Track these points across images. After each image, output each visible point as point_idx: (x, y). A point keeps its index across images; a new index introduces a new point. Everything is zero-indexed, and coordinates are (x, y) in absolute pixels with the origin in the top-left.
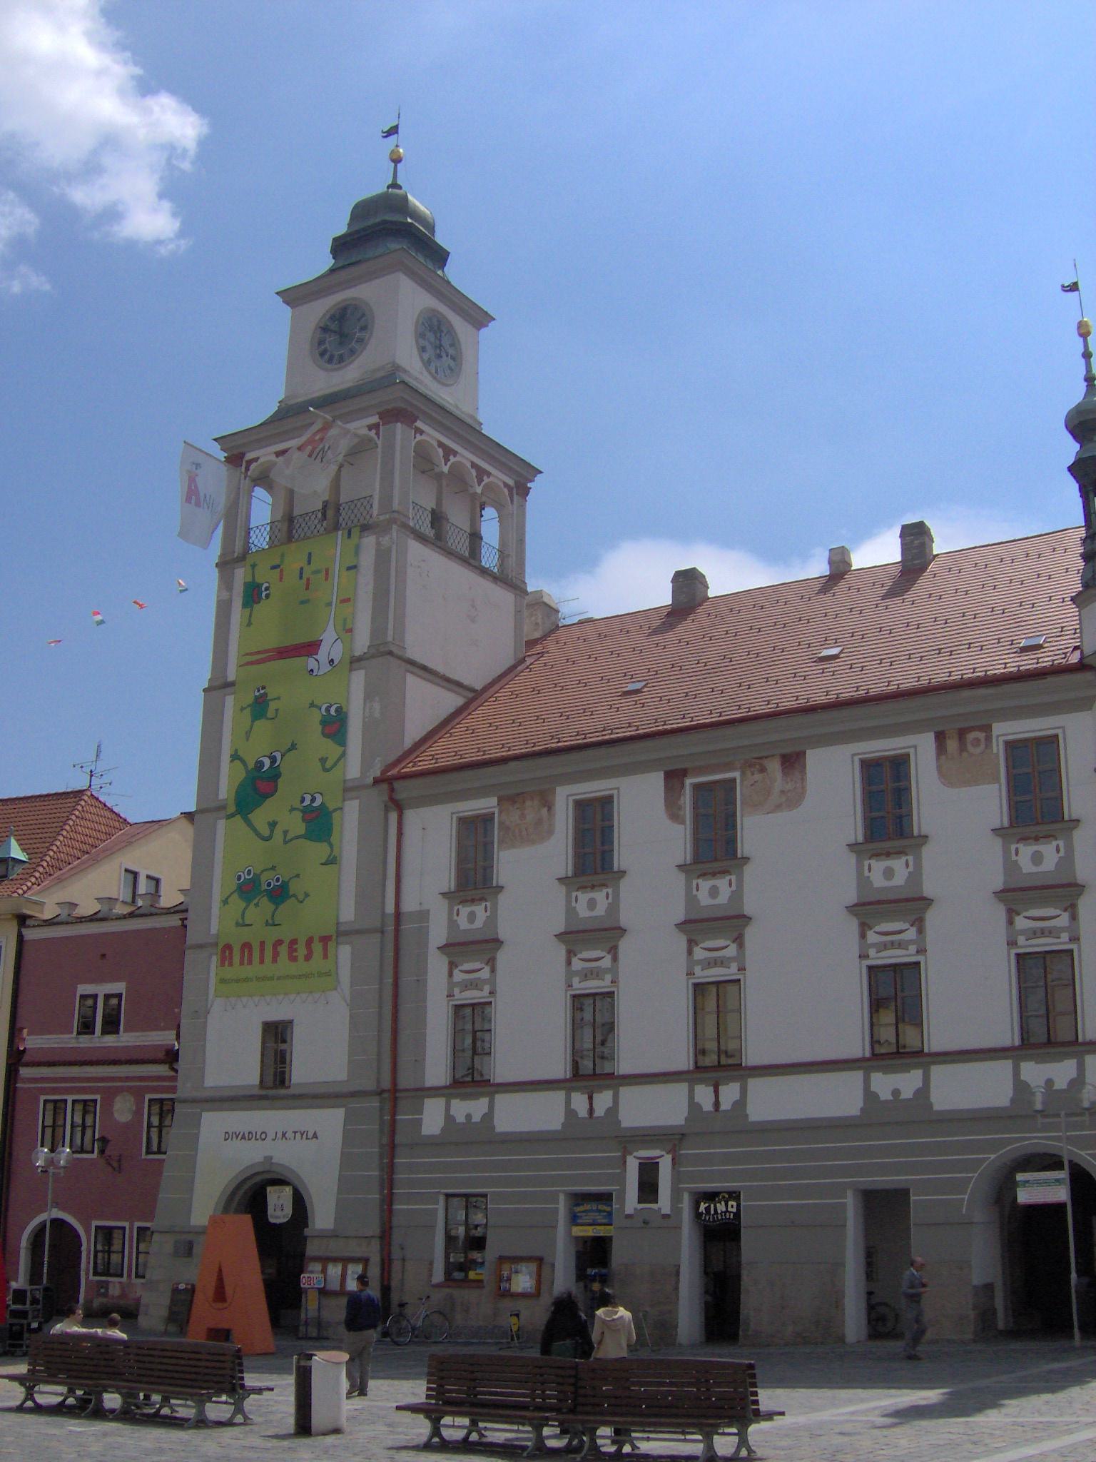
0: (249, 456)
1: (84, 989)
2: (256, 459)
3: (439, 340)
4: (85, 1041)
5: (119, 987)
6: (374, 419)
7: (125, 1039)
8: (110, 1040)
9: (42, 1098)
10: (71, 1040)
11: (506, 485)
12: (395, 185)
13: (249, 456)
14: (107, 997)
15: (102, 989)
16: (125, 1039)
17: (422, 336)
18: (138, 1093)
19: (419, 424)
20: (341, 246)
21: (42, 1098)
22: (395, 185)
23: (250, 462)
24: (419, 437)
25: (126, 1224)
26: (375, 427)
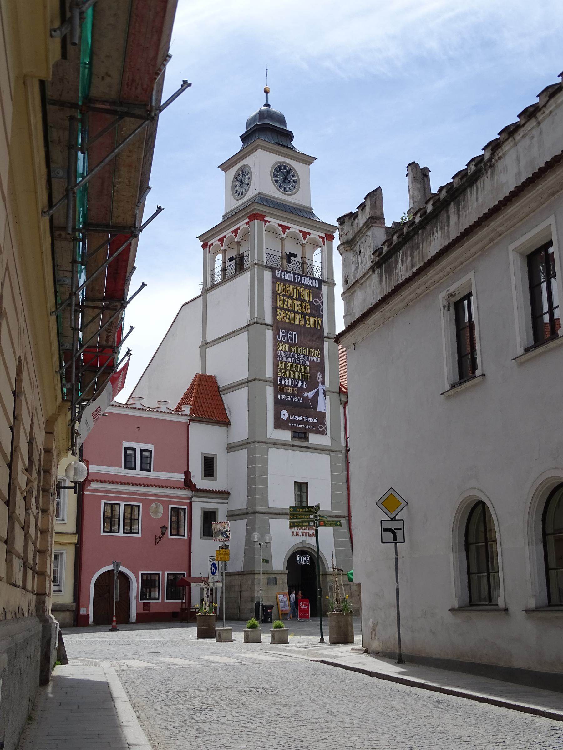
0: (210, 243)
1: (126, 444)
2: (212, 244)
3: (285, 176)
4: (130, 472)
5: (150, 447)
6: (247, 220)
7: (154, 474)
8: (145, 474)
9: (103, 502)
10: (120, 471)
11: (320, 237)
12: (267, 105)
13: (210, 243)
14: (142, 451)
15: (139, 446)
16: (154, 474)
17: (275, 176)
18: (165, 504)
19: (267, 218)
20: (245, 138)
21: (103, 502)
22: (267, 105)
23: (210, 246)
24: (267, 224)
25: (160, 573)
26: (247, 224)
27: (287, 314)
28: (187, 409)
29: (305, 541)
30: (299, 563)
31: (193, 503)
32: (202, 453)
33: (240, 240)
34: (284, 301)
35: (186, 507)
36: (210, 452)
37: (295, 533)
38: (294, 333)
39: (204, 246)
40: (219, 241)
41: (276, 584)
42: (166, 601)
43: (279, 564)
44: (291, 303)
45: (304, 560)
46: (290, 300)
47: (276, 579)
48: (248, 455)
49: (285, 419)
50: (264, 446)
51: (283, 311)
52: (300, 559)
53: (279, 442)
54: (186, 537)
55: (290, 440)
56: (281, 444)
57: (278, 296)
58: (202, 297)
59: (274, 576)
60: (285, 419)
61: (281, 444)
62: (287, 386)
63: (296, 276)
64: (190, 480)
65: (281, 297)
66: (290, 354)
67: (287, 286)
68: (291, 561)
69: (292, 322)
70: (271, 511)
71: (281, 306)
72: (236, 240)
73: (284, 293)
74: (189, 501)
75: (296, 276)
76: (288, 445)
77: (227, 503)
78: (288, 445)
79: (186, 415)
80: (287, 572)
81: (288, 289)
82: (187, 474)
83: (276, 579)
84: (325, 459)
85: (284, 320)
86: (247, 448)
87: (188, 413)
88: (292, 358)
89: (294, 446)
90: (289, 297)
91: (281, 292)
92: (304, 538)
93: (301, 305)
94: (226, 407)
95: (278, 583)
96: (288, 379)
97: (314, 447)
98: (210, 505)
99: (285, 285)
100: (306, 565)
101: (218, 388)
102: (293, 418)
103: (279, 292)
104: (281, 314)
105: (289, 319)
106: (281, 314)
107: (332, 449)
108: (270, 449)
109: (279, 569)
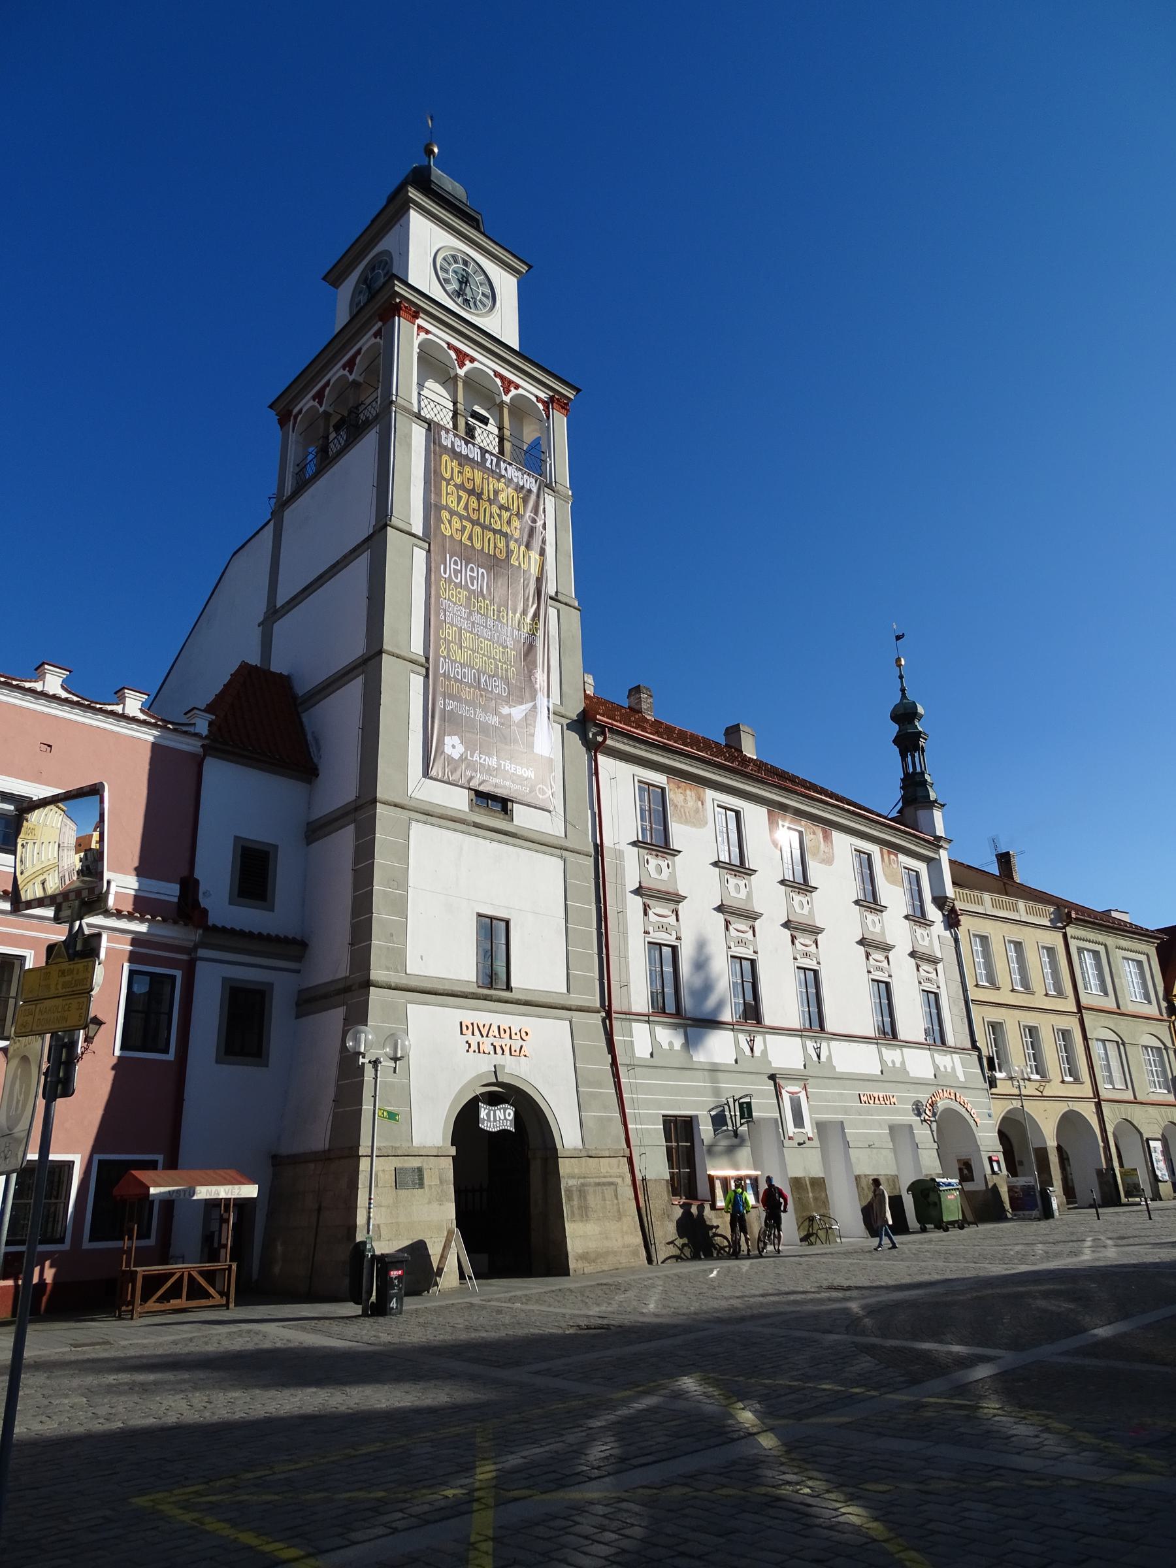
2: (300, 411)
23: (296, 417)
26: (378, 334)
27: (464, 528)
28: (202, 725)
29: (503, 1067)
30: (484, 1126)
31: (199, 964)
32: (236, 838)
33: (361, 379)
34: (459, 498)
35: (178, 974)
36: (258, 833)
37: (474, 1047)
38: (481, 570)
39: (283, 422)
40: (314, 398)
41: (421, 1185)
42: (86, 1245)
43: (431, 1129)
44: (475, 505)
45: (498, 1119)
46: (473, 499)
47: (420, 1170)
48: (357, 838)
49: (456, 756)
50: (405, 815)
51: (455, 519)
52: (488, 1115)
53: (439, 811)
54: (171, 1056)
55: (465, 807)
56: (442, 817)
57: (444, 483)
58: (272, 523)
59: (415, 1163)
60: (456, 756)
61: (442, 817)
62: (461, 681)
63: (487, 455)
64: (196, 903)
65: (451, 488)
66: (470, 614)
67: (467, 468)
68: (465, 1121)
69: (478, 546)
70: (414, 983)
71: (452, 506)
72: (351, 378)
73: (458, 481)
74: (185, 957)
75: (487, 455)
76: (463, 822)
77: (298, 971)
78: (463, 822)
79: (196, 735)
80: (453, 1151)
81: (470, 475)
82: (189, 886)
83: (420, 1170)
84: (551, 866)
85: (457, 537)
86: (355, 821)
87: (205, 732)
88: (473, 623)
89: (476, 825)
90: (471, 492)
91: (452, 478)
92: (499, 1059)
93: (500, 516)
94: (309, 737)
95: (426, 1182)
96: (463, 665)
97: (525, 834)
98: (249, 972)
99: (460, 465)
100: (504, 1132)
101: (294, 697)
102: (476, 757)
103: (448, 476)
104: (450, 522)
105: (470, 538)
106: (450, 522)
107: (567, 844)
108: (414, 825)
109: (429, 1143)
